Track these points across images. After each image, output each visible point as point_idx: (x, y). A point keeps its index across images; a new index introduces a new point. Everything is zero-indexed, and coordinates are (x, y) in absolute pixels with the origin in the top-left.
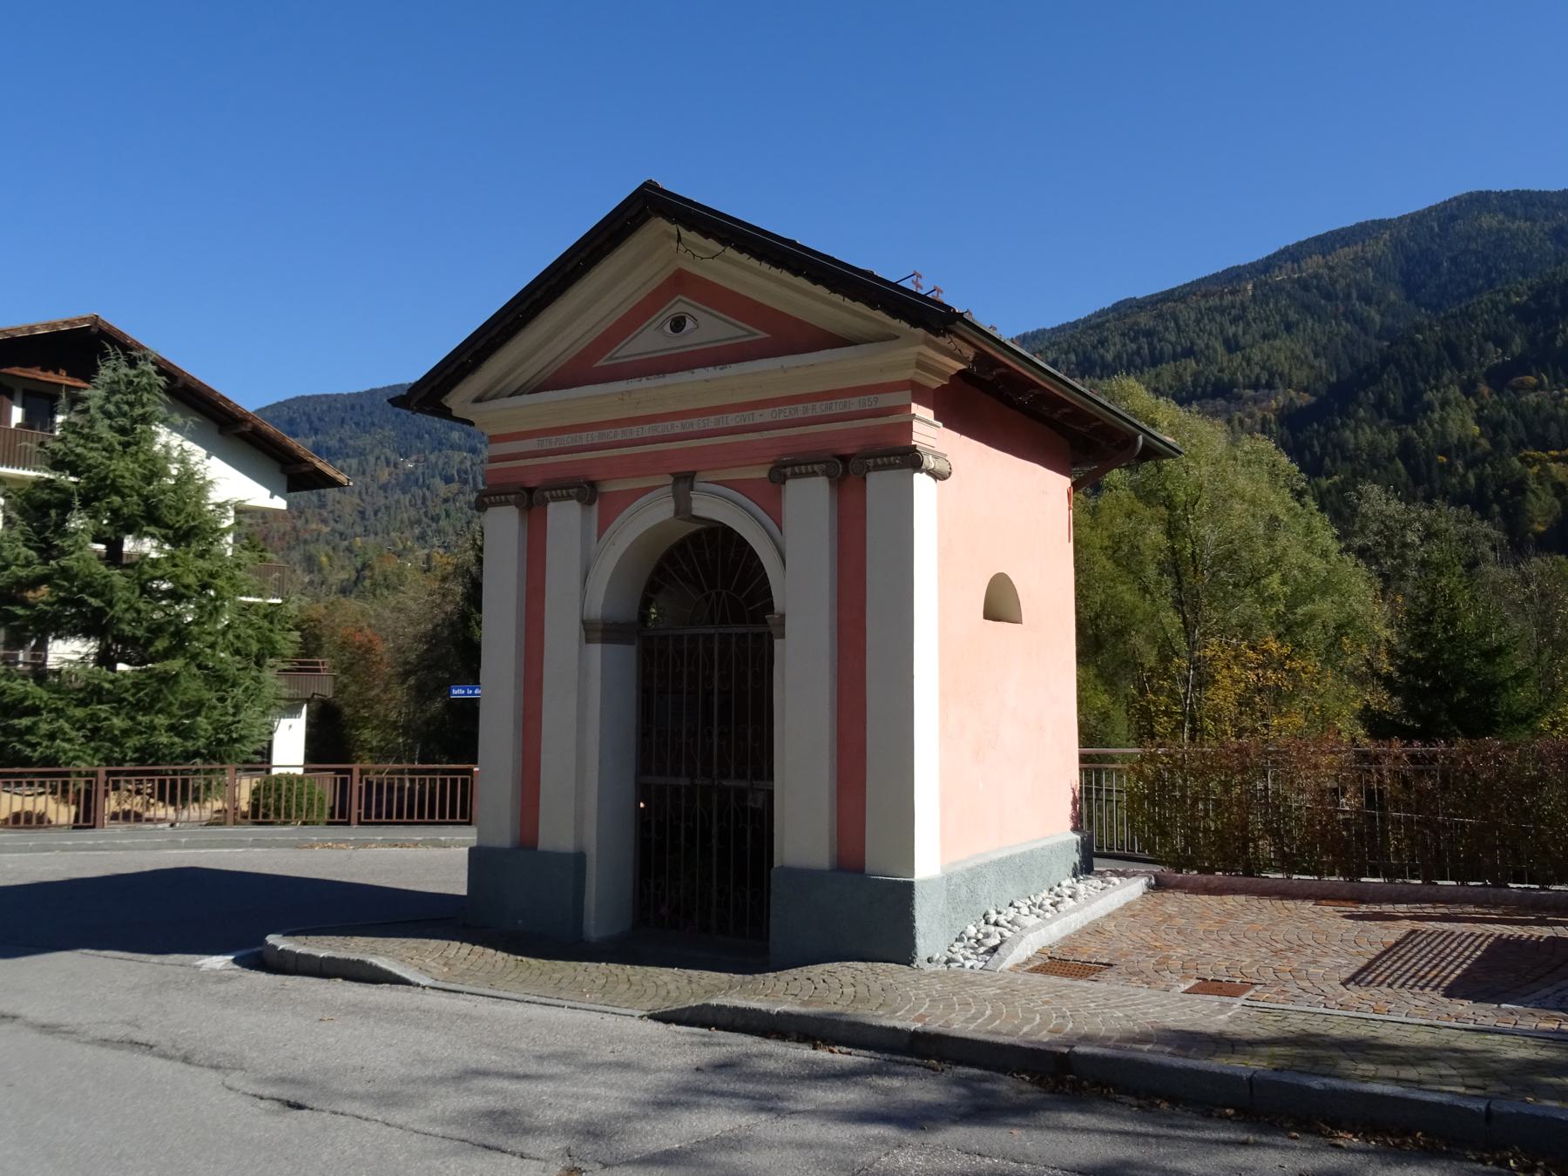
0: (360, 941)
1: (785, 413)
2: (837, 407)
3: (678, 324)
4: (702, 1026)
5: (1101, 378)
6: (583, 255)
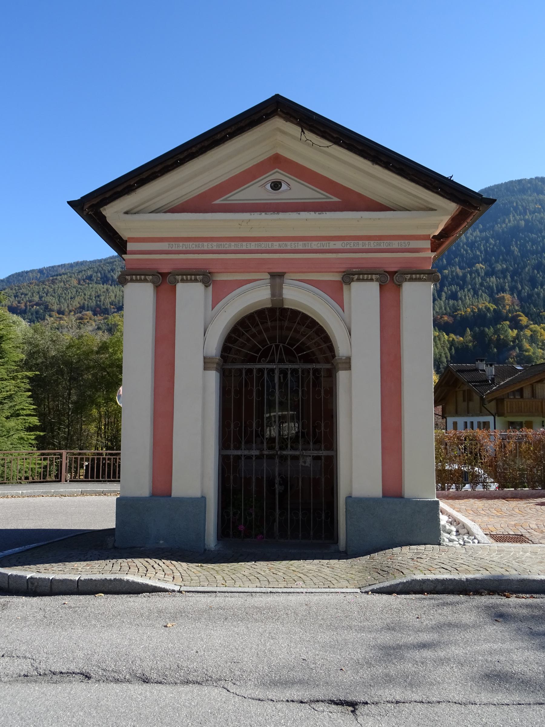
0: (56, 566)
1: (351, 245)
2: (384, 245)
3: (276, 186)
4: (415, 593)
5: (111, 285)
6: (229, 130)
